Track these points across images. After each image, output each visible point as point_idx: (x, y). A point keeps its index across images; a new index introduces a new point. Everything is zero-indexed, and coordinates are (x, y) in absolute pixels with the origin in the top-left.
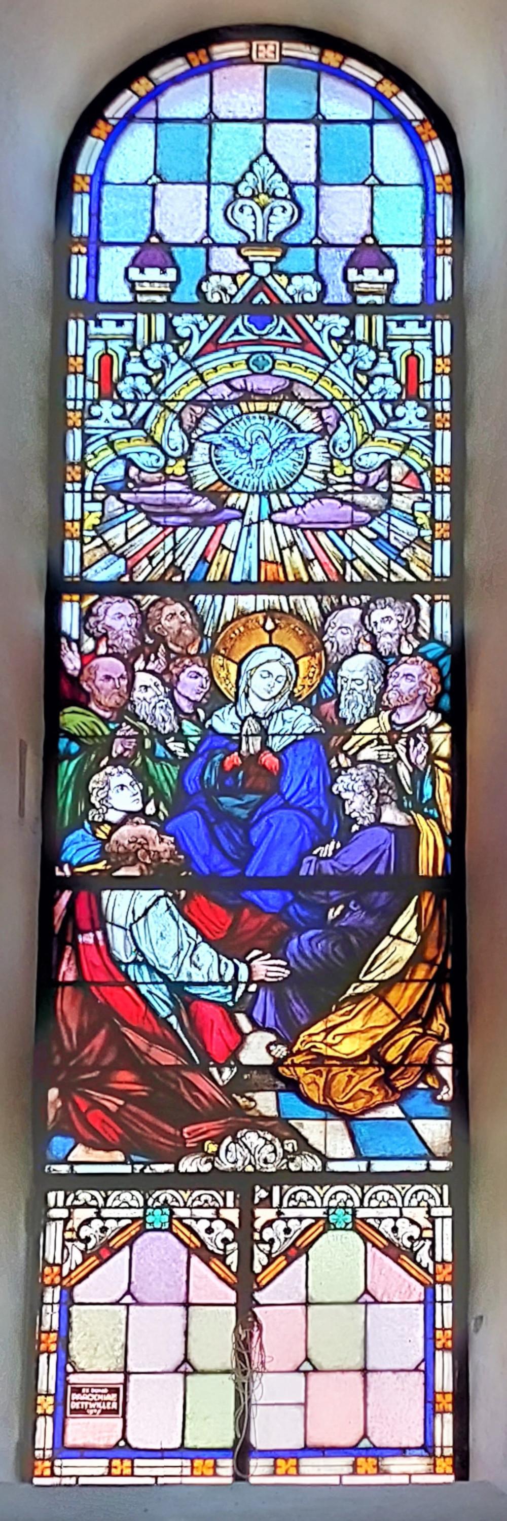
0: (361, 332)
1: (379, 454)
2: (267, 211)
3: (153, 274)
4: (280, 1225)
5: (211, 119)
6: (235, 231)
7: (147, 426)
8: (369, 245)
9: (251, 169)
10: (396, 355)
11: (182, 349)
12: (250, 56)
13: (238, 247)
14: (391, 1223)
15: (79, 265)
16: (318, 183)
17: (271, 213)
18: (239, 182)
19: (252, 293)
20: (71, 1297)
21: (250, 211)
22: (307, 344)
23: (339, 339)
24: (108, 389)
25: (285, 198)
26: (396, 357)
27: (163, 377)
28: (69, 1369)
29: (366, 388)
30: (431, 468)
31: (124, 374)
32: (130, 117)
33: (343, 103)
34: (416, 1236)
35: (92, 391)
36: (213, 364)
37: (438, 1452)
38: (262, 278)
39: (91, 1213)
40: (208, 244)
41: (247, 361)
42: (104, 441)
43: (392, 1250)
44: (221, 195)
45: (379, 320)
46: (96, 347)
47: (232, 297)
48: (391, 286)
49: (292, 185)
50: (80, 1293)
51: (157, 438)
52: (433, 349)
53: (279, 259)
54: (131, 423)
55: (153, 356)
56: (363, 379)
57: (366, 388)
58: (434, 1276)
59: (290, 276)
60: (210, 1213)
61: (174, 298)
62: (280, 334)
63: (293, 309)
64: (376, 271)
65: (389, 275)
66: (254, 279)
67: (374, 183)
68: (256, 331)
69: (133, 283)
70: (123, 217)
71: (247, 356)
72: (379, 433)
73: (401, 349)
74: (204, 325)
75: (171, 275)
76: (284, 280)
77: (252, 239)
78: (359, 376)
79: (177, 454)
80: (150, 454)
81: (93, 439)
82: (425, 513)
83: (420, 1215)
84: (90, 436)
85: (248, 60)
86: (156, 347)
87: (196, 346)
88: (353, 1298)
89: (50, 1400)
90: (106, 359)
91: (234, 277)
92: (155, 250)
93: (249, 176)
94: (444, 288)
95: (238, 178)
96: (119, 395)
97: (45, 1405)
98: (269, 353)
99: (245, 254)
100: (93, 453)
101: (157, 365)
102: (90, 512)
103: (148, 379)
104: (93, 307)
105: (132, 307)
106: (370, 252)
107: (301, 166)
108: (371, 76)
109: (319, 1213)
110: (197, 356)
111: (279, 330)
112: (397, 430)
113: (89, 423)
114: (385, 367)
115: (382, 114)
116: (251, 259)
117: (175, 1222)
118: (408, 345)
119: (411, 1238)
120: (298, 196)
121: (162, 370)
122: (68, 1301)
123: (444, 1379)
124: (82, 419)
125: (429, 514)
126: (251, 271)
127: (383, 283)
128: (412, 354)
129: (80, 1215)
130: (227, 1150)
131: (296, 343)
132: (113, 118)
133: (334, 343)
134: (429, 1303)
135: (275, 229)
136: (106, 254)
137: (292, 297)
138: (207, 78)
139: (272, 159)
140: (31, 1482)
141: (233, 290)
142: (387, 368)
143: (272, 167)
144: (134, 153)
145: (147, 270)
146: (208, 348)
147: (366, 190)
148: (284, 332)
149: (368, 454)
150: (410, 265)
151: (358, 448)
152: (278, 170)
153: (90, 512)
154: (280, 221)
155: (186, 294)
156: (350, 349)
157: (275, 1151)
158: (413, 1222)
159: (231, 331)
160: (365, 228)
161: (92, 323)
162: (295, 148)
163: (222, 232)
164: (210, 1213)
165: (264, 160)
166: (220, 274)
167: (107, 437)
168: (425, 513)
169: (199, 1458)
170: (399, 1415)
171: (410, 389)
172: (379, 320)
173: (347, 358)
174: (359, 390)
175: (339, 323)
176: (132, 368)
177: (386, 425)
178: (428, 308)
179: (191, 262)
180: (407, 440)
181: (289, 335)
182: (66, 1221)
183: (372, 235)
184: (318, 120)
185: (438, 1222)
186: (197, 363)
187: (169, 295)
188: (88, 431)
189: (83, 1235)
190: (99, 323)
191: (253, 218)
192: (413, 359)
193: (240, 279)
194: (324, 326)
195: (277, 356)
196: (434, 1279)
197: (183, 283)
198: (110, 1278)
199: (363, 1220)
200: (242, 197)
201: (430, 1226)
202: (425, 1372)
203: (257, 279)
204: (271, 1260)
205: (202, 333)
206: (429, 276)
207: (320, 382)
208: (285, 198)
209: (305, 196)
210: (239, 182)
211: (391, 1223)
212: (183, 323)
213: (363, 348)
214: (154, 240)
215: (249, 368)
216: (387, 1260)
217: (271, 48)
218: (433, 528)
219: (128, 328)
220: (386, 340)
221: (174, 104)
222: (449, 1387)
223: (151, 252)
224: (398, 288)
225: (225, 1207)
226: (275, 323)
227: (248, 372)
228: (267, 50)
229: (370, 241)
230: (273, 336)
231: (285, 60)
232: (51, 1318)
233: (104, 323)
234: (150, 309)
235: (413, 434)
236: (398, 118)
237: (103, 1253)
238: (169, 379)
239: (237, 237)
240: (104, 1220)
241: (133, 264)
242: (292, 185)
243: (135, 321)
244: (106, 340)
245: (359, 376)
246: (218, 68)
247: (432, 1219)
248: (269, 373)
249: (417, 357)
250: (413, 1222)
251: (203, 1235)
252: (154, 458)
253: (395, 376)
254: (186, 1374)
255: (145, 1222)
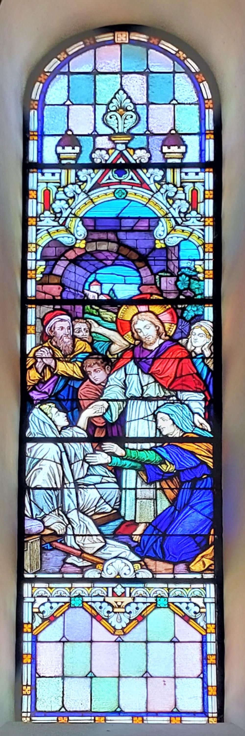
0: (169, 178)
1: (178, 237)
2: (124, 117)
3: (68, 149)
4: (134, 606)
5: (95, 72)
6: (108, 128)
7: (66, 225)
8: (173, 134)
9: (114, 97)
10: (186, 189)
11: (82, 187)
12: (114, 40)
13: (110, 136)
14: (186, 605)
15: (33, 146)
16: (148, 104)
17: (126, 119)
18: (109, 104)
19: (117, 158)
20: (37, 639)
21: (115, 118)
22: (142, 184)
23: (159, 182)
24: (48, 206)
25: (131, 110)
26: (187, 191)
27: (74, 201)
28: (37, 676)
29: (171, 206)
30: (204, 244)
31: (55, 200)
32: (57, 72)
33: (159, 62)
34: (197, 611)
35: (41, 208)
36: (97, 194)
37: (210, 715)
38: (121, 152)
39: (45, 600)
40: (95, 135)
41: (114, 193)
42: (46, 232)
43: (186, 618)
44: (101, 110)
45: (72, 172)
46: (42, 186)
47: (106, 161)
48: (184, 154)
49: (135, 105)
50: (40, 638)
51: (72, 231)
52: (204, 186)
53: (129, 141)
54: (59, 223)
55: (69, 190)
56: (171, 202)
57: (171, 206)
58: (206, 630)
59: (134, 150)
60: (187, 600)
61: (80, 162)
62: (130, 179)
63: (135, 167)
64: (71, 148)
65: (183, 149)
66: (117, 152)
67: (174, 102)
68: (117, 177)
69: (164, 154)
70: (54, 123)
71: (113, 190)
72: (177, 227)
73: (189, 187)
74: (93, 175)
75: (77, 149)
76: (131, 152)
77: (117, 132)
78: (169, 200)
79: (81, 238)
80: (69, 237)
81: (41, 230)
82: (200, 265)
83: (200, 601)
84: (39, 229)
85: (113, 43)
86: (70, 186)
87: (88, 186)
88: (62, 103)
89: (29, 688)
90: (47, 193)
91: (107, 151)
92: (69, 139)
93: (114, 100)
94: (210, 156)
95: (109, 100)
96: (53, 209)
97: (27, 690)
98: (124, 189)
99: (113, 139)
100: (41, 237)
101: (72, 195)
102: (40, 266)
103: (67, 202)
104: (40, 166)
105: (59, 166)
106: (174, 138)
107: (139, 96)
108: (172, 49)
109: (153, 600)
110: (90, 191)
111: (130, 177)
112: (187, 226)
113: (39, 223)
114: (181, 195)
115: (179, 68)
116: (116, 142)
117: (85, 604)
118: (192, 185)
119: (195, 613)
120: (138, 110)
121: (74, 197)
122: (35, 641)
123: (212, 680)
124: (36, 221)
125: (203, 266)
126: (115, 149)
127: (74, 153)
128: (194, 189)
129: (40, 601)
130: (107, 569)
131: (138, 184)
132: (48, 72)
133: (156, 184)
134: (203, 643)
135: (128, 126)
136: (46, 140)
137: (135, 160)
138: (93, 50)
139: (125, 92)
140: (21, 720)
141: (107, 157)
142: (183, 196)
143: (125, 95)
144: (57, 92)
145: (66, 148)
146: (95, 186)
147: (172, 106)
148: (132, 178)
149: (172, 238)
150: (193, 142)
151: (168, 234)
152: (129, 97)
153: (40, 266)
154: (130, 122)
155: (84, 159)
156: (164, 186)
157: (130, 569)
158: (196, 605)
159: (107, 177)
160: (171, 126)
161: (40, 174)
162: (136, 86)
163: (102, 129)
164: (102, 599)
165: (121, 92)
166: (101, 149)
167: (47, 230)
168: (200, 265)
169: (98, 716)
170: (190, 697)
171: (193, 205)
172: (177, 171)
173: (162, 191)
174: (168, 206)
175: (158, 174)
176: (59, 196)
177: (182, 223)
178: (203, 165)
179: (87, 143)
180: (191, 230)
181: (134, 180)
182: (33, 603)
183: (174, 129)
184: (147, 73)
185: (208, 605)
186: (90, 194)
187: (76, 159)
188: (38, 228)
189: (41, 610)
190: (43, 174)
191: (116, 121)
192: (194, 192)
193: (110, 152)
194: (151, 175)
195: (128, 190)
196: (206, 630)
197: (83, 153)
198: (53, 632)
199: (173, 603)
200: (111, 111)
201: (204, 606)
202: (203, 679)
203: (118, 152)
204: (131, 621)
205: (92, 178)
206: (202, 151)
207: (150, 203)
208: (131, 110)
209: (142, 110)
210: (109, 104)
211: (186, 605)
212: (83, 174)
213: (171, 186)
214: (69, 133)
215: (114, 196)
216: (182, 621)
217: (125, 35)
218: (204, 273)
219: (57, 176)
220: (181, 183)
221: (76, 65)
222: (215, 683)
223: (66, 139)
224: (187, 155)
225: (107, 596)
226: (127, 174)
227: (114, 198)
228: (122, 37)
229: (173, 132)
230: (126, 180)
231: (131, 42)
232: (27, 648)
233: (45, 174)
234: (68, 167)
235: (195, 228)
236: (187, 71)
237: (52, 619)
238: (77, 202)
239: (110, 132)
240: (51, 603)
241: (163, 145)
242: (135, 105)
243: (60, 173)
244: (47, 183)
245: (169, 200)
246: (99, 47)
247: (205, 603)
248: (124, 198)
249: (49, 191)
250: (196, 605)
251: (98, 610)
252: (70, 239)
253: (185, 199)
254: (91, 677)
255: (71, 604)
